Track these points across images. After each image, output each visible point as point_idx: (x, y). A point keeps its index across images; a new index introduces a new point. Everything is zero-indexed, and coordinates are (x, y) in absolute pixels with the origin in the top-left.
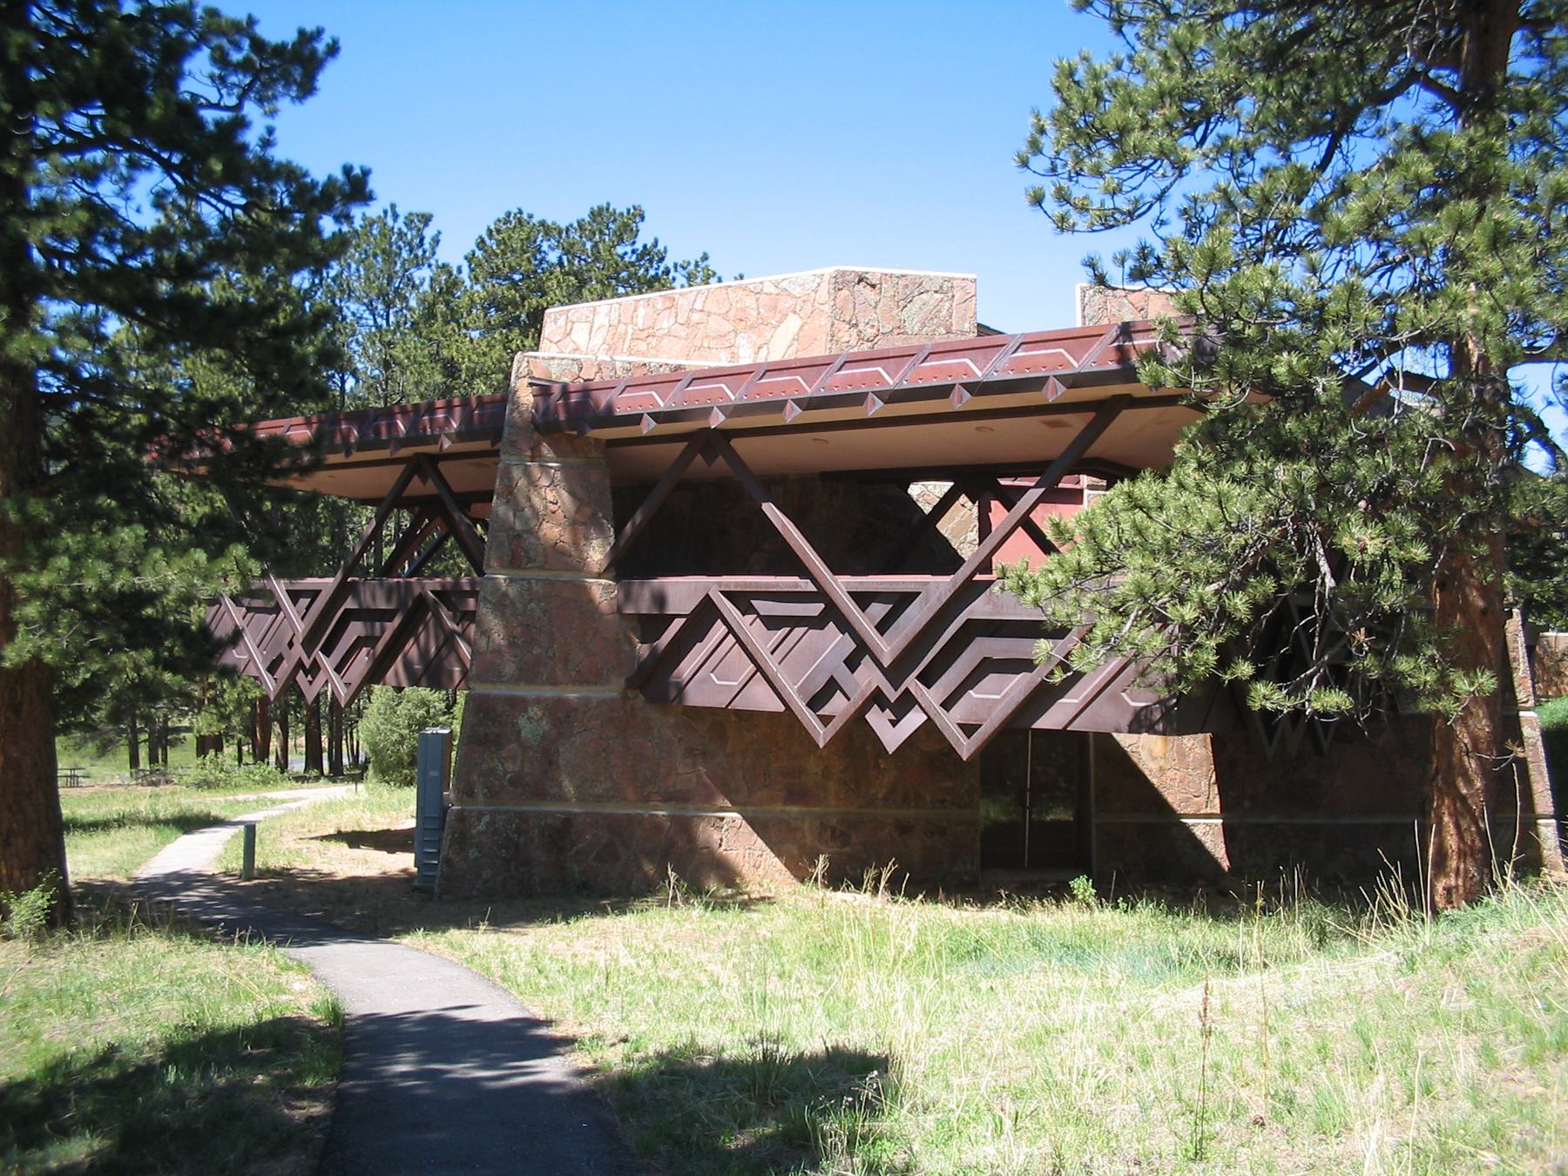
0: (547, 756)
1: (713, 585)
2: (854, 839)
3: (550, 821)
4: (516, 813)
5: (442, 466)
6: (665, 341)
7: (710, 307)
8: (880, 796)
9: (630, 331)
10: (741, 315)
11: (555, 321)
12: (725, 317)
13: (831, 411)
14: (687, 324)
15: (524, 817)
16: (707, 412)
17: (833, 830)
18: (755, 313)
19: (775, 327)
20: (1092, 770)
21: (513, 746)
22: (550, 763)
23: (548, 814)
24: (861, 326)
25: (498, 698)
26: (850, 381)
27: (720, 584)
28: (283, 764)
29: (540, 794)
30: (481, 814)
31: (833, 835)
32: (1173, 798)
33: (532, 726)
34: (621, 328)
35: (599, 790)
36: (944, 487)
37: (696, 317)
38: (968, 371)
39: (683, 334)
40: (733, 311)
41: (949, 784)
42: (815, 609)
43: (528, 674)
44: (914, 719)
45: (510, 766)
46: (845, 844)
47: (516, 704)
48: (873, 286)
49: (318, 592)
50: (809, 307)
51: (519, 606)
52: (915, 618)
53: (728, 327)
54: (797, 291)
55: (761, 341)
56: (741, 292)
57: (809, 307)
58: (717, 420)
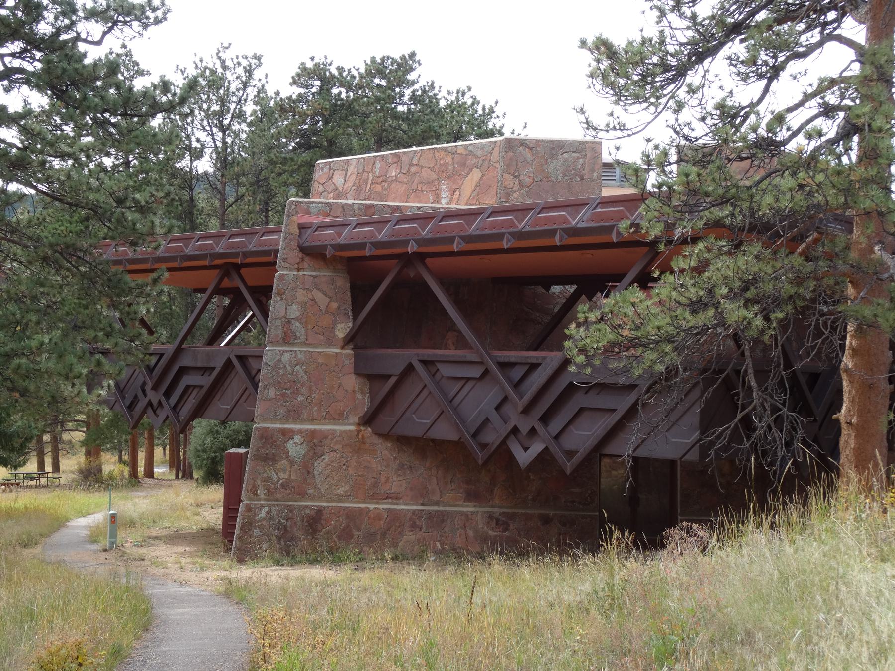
0: (307, 470)
1: (412, 355)
2: (511, 527)
3: (308, 512)
4: (285, 505)
5: (243, 271)
6: (393, 185)
7: (423, 162)
8: (530, 497)
9: (371, 178)
10: (443, 168)
11: (322, 169)
12: (432, 169)
13: (482, 246)
14: (408, 173)
15: (291, 509)
16: (407, 242)
17: (497, 521)
18: (451, 167)
19: (465, 177)
20: (679, 482)
21: (284, 462)
22: (309, 473)
23: (307, 507)
24: (521, 177)
25: (274, 429)
26: (494, 225)
27: (418, 355)
28: (149, 474)
29: (303, 495)
30: (262, 506)
31: (497, 524)
32: (155, 459)
33: (295, 448)
34: (365, 175)
35: (340, 491)
36: (572, 288)
37: (413, 169)
38: (566, 221)
39: (405, 180)
40: (438, 165)
41: (577, 490)
42: (476, 372)
43: (294, 414)
44: (537, 448)
45: (282, 475)
46: (505, 530)
47: (287, 434)
48: (530, 149)
49: (162, 355)
50: (486, 163)
51: (289, 368)
52: (538, 379)
53: (434, 176)
54: (479, 153)
55: (455, 187)
56: (443, 152)
57: (486, 163)
58: (412, 248)
